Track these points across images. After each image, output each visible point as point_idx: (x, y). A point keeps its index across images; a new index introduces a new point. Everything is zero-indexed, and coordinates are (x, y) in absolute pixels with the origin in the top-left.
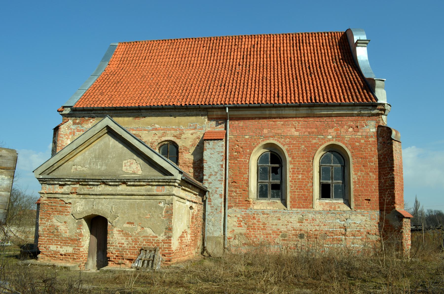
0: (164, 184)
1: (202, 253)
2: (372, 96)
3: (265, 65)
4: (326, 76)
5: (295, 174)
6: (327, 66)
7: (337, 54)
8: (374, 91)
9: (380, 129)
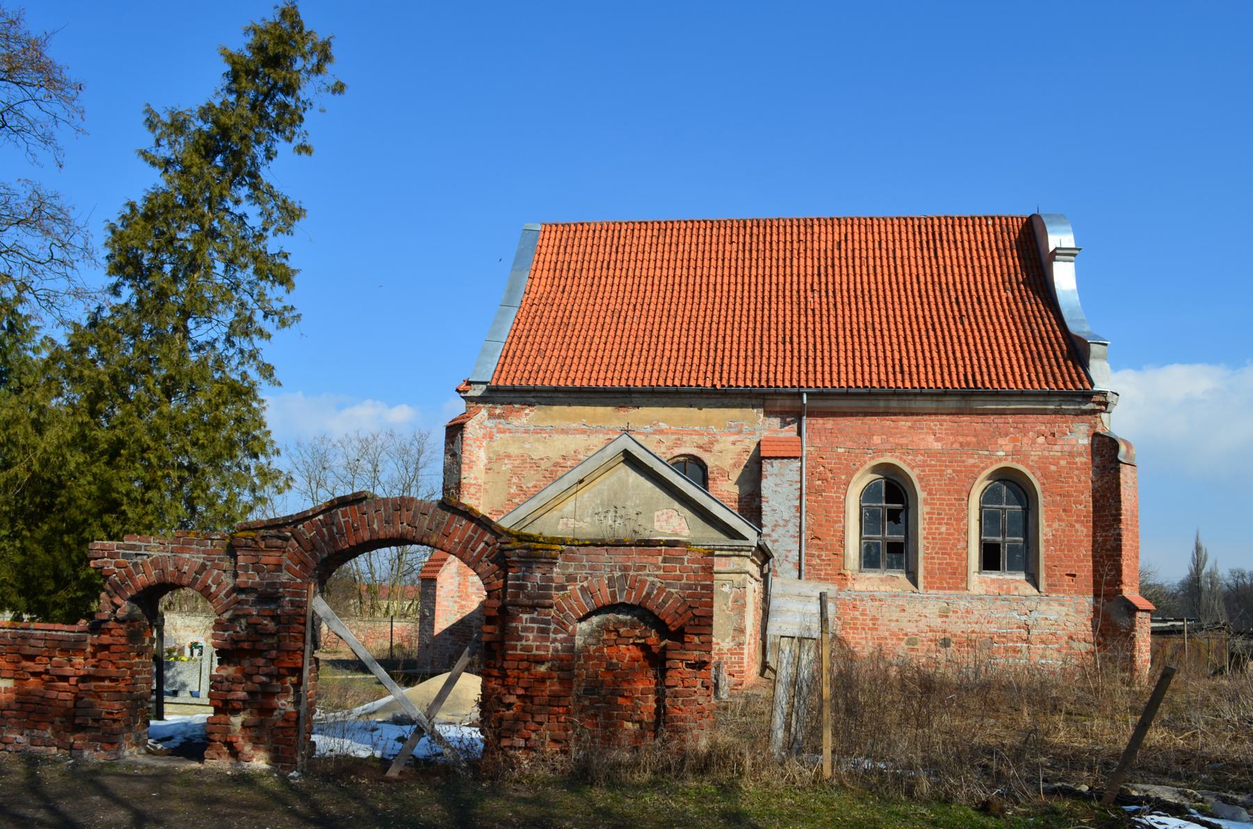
0: (731, 553)
1: (762, 674)
2: (1083, 375)
3: (866, 292)
4: (993, 324)
5: (934, 524)
6: (993, 298)
7: (1012, 270)
8: (1088, 365)
9: (1097, 439)
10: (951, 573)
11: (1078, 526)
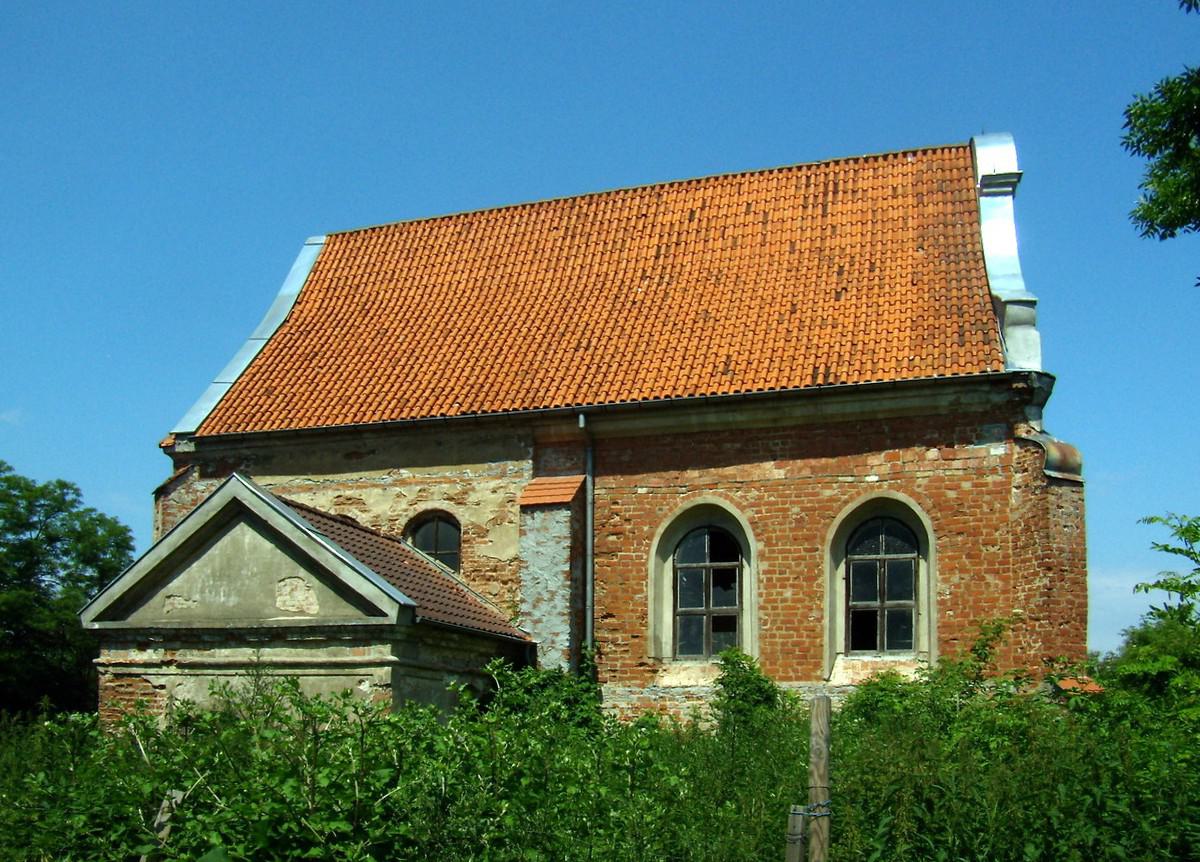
5: (775, 586)
10: (799, 657)
11: (989, 578)
